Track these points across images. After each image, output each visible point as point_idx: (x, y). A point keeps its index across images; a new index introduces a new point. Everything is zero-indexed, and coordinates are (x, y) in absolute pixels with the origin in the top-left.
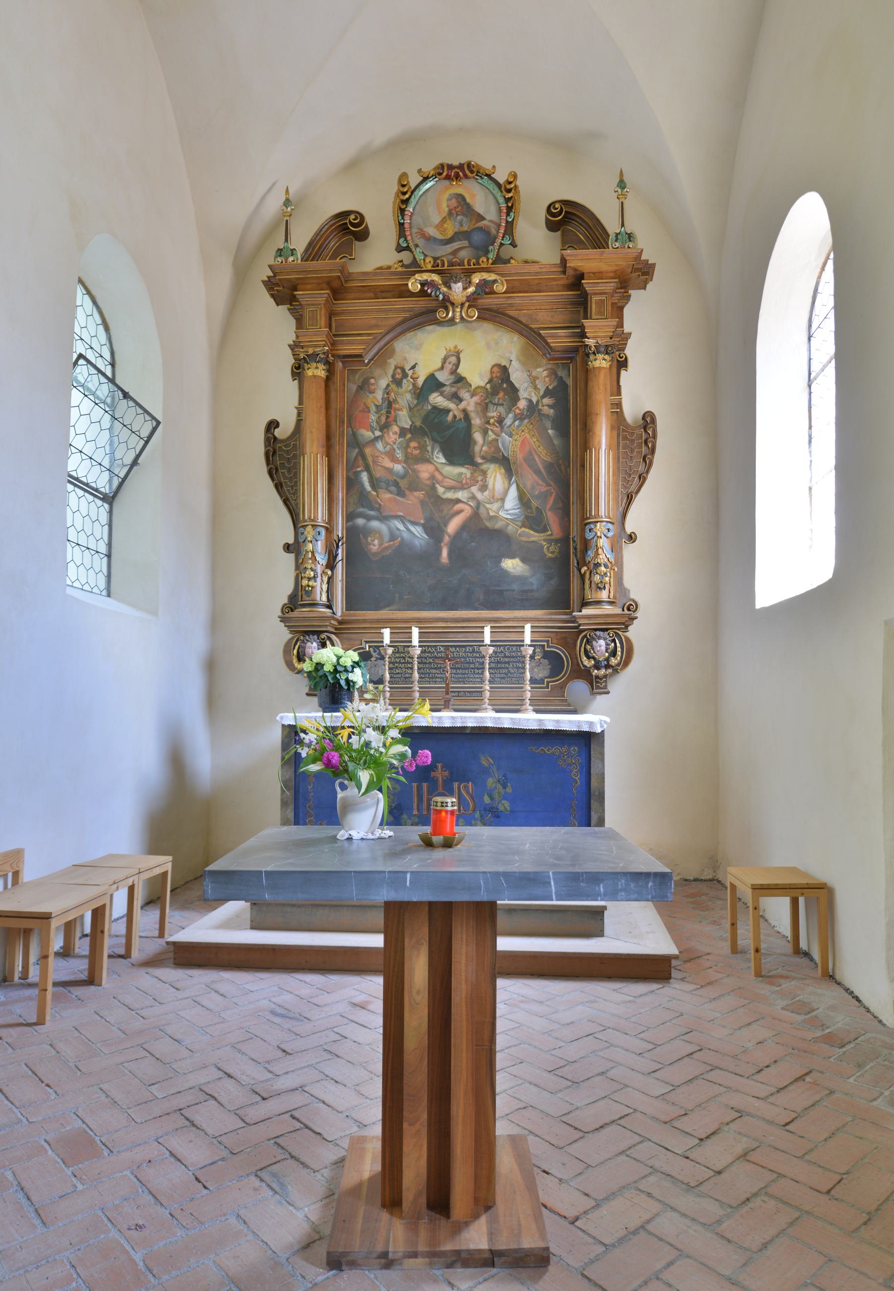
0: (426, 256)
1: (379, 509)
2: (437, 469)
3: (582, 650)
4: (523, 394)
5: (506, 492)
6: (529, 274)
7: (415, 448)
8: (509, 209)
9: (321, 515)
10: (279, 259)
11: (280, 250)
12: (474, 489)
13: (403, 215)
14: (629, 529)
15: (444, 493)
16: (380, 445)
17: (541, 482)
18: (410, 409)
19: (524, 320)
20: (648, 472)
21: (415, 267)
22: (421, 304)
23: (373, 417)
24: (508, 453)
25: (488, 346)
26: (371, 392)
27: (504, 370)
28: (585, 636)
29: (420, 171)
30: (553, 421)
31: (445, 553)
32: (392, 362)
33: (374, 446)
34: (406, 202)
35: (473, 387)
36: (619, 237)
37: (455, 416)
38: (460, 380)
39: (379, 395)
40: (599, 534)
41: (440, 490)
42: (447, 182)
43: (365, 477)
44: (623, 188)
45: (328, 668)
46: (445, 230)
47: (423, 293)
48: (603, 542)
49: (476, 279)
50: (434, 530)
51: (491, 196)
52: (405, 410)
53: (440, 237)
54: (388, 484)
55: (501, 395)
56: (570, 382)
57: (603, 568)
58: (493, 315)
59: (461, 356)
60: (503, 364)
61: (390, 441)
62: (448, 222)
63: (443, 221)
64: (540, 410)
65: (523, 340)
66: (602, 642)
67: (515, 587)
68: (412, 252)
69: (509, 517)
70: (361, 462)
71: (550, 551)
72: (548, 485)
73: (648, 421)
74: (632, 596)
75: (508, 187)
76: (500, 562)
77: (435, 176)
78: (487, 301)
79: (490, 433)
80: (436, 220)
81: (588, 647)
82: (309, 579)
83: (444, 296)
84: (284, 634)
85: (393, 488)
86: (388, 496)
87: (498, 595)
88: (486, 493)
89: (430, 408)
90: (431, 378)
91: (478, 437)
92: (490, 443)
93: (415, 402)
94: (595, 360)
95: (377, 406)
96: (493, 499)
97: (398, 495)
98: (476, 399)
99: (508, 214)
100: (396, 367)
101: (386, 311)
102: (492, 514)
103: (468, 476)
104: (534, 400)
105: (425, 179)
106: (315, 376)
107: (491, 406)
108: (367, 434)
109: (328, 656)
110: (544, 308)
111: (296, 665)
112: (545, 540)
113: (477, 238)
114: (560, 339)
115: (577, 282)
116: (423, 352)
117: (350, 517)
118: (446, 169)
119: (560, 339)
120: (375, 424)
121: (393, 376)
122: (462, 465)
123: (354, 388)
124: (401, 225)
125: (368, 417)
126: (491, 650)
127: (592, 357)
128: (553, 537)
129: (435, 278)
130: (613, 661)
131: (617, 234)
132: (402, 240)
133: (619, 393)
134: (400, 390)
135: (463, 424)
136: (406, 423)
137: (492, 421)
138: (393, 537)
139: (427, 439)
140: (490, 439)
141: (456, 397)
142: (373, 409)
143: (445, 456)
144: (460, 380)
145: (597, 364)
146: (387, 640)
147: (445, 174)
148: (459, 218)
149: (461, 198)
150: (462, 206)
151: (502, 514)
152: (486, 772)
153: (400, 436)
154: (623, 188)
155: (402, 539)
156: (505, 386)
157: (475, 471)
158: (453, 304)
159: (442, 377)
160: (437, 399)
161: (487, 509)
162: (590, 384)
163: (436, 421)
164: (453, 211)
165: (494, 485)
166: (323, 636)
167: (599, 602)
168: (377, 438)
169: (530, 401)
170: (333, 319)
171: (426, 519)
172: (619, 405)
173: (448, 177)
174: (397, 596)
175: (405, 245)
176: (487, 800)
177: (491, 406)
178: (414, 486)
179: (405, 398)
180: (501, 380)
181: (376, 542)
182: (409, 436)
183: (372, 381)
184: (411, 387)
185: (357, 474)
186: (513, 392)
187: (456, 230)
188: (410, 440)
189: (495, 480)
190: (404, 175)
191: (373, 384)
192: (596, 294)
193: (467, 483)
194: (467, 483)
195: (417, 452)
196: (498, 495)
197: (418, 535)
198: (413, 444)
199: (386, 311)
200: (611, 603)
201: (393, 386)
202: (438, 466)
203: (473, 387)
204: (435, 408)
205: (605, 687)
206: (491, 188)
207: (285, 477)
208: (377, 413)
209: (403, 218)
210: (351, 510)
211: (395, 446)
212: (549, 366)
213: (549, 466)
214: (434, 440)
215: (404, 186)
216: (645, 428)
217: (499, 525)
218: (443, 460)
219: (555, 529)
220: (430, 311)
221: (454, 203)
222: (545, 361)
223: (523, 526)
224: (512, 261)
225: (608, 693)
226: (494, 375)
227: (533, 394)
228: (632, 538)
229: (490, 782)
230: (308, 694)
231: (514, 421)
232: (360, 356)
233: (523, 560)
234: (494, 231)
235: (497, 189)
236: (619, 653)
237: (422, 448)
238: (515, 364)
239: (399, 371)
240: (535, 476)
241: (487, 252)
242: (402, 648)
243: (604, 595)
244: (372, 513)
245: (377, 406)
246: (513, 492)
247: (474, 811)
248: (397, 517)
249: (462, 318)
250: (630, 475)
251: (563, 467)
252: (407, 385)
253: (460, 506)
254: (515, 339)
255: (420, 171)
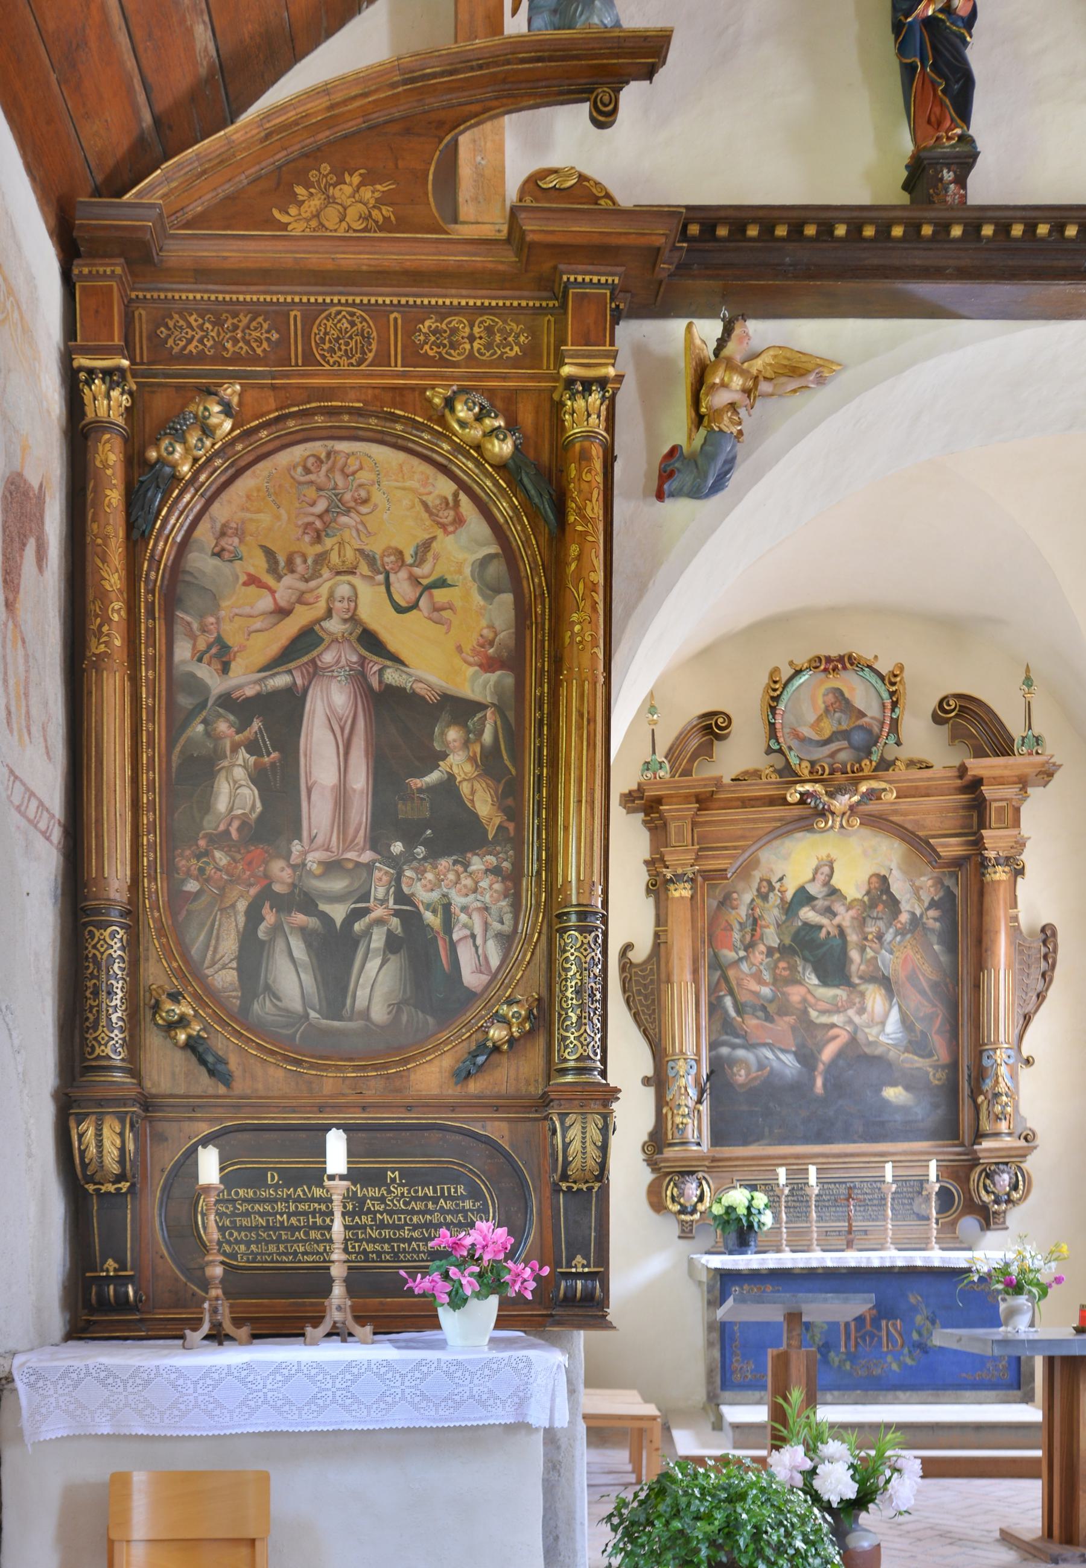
0: (801, 759)
1: (745, 1036)
2: (809, 991)
3: (981, 1185)
4: (905, 906)
5: (887, 1015)
6: (921, 780)
7: (784, 969)
8: (895, 704)
9: (690, 1048)
10: (650, 774)
11: (647, 763)
12: (851, 1012)
13: (774, 714)
14: (1025, 1055)
15: (818, 1017)
16: (744, 967)
17: (926, 1003)
18: (778, 926)
19: (909, 826)
20: (1047, 989)
21: (788, 774)
22: (797, 811)
23: (736, 936)
24: (889, 972)
25: (865, 853)
26: (733, 908)
27: (884, 880)
28: (985, 1170)
29: (791, 663)
30: (939, 936)
31: (819, 1082)
32: (757, 875)
33: (739, 967)
34: (776, 699)
35: (849, 900)
36: (1026, 740)
37: (828, 933)
38: (834, 892)
39: (743, 911)
40: (999, 1061)
41: (813, 1014)
42: (823, 675)
43: (728, 1002)
44: (1029, 686)
45: (742, 1211)
46: (822, 730)
47: (802, 802)
48: (1003, 1070)
49: (863, 788)
50: (807, 1058)
51: (873, 690)
52: (772, 927)
53: (816, 737)
54: (754, 1008)
55: (881, 907)
56: (958, 892)
57: (1004, 1098)
58: (877, 822)
59: (835, 865)
60: (882, 873)
61: (756, 962)
62: (825, 720)
63: (819, 719)
64: (924, 924)
65: (905, 846)
66: (1006, 1176)
67: (898, 1117)
68: (785, 756)
69: (890, 1042)
70: (723, 985)
71: (937, 1078)
72: (934, 1005)
73: (1048, 934)
74: (1029, 1125)
75: (893, 680)
76: (881, 1090)
77: (809, 668)
78: (872, 807)
79: (868, 950)
80: (811, 718)
81: (988, 1182)
82: (683, 1116)
83: (824, 805)
84: (647, 1176)
85: (760, 1014)
86: (755, 1022)
87: (878, 1127)
88: (865, 1016)
89: (800, 924)
90: (802, 891)
91: (854, 954)
92: (868, 961)
93: (784, 918)
94: (995, 873)
95: (740, 923)
96: (871, 1023)
97: (766, 1020)
98: (852, 913)
99: (893, 711)
100: (762, 880)
101: (754, 821)
102: (871, 1039)
103: (845, 997)
104: (918, 913)
105: (798, 672)
106: (682, 898)
107: (869, 921)
108: (729, 955)
109: (738, 1198)
110: (934, 814)
111: (670, 1207)
112: (930, 1066)
113: (858, 738)
114: (951, 847)
115: (975, 785)
116: (794, 862)
117: (713, 1046)
118: (823, 662)
119: (951, 847)
120: (738, 944)
121: (758, 890)
122: (837, 986)
123: (715, 903)
124: (772, 726)
125: (731, 936)
126: (894, 1187)
127: (990, 870)
128: (940, 1063)
129: (818, 788)
130: (1015, 1195)
131: (1023, 738)
132: (773, 741)
133: (1016, 907)
134: (766, 905)
135: (838, 941)
136: (774, 942)
137: (870, 937)
138: (761, 1066)
139: (797, 959)
140: (868, 957)
141: (830, 912)
142: (736, 926)
143: (819, 978)
144: (834, 892)
145: (997, 877)
146: (782, 1180)
147: (822, 667)
148: (837, 715)
149: (838, 693)
150: (841, 702)
151: (882, 1038)
152: (914, 1309)
153: (767, 956)
154: (1029, 686)
155: (772, 1068)
156: (884, 897)
157: (851, 992)
158: (833, 813)
159: (814, 889)
160: (807, 914)
161: (866, 1034)
162: (987, 899)
163: (807, 938)
164: (831, 708)
165: (873, 1007)
166: (700, 1175)
167: (997, 1134)
168: (741, 959)
169: (913, 914)
170: (695, 831)
171: (797, 1046)
172: (1015, 919)
173: (825, 670)
174: (767, 1129)
175: (776, 747)
176: (915, 1336)
177: (869, 921)
178: (784, 1009)
179: (772, 913)
180: (881, 892)
181: (743, 1072)
182: (777, 955)
183: (735, 895)
184: (779, 901)
185: (720, 999)
186: (894, 904)
187: (834, 729)
188: (779, 960)
189: (874, 1002)
190: (776, 670)
191: (735, 900)
192: (995, 800)
193: (843, 1006)
194: (843, 1006)
195: (786, 973)
196: (877, 1019)
197: (788, 1064)
198: (782, 965)
199: (754, 821)
200: (1010, 1134)
201: (758, 901)
202: (810, 988)
203: (849, 900)
204: (806, 924)
205: (1004, 1223)
206: (874, 682)
207: (642, 1005)
208: (741, 930)
209: (774, 718)
210: (713, 1038)
211: (762, 968)
212: (935, 875)
213: (935, 986)
214: (805, 959)
215: (775, 682)
216: (1045, 942)
217: (878, 1051)
218: (816, 981)
219: (942, 1054)
220: (811, 816)
221: (831, 698)
222: (929, 869)
223: (907, 1051)
224: (898, 763)
225: (1007, 1228)
226: (872, 886)
227: (916, 906)
228: (1028, 1062)
229: (919, 1319)
230: (680, 1237)
231: (896, 936)
232: (725, 870)
233: (907, 1088)
234: (876, 730)
235: (880, 682)
236: (1021, 1187)
237: (793, 968)
238: (896, 873)
239: (765, 884)
240: (919, 997)
241: (869, 753)
242: (798, 1188)
243: (1003, 1126)
244: (737, 1041)
245: (740, 923)
246: (894, 1015)
247: (902, 1346)
248: (765, 1045)
249: (842, 826)
250: (1026, 993)
251: (950, 986)
252: (774, 899)
253: (834, 1032)
254: (896, 846)
255: (791, 663)
